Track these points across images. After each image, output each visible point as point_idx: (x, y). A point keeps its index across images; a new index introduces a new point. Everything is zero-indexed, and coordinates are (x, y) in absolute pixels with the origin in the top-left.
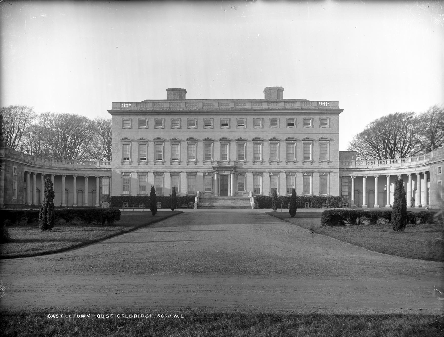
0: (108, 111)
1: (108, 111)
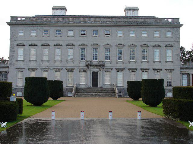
0: (183, 24)
1: (183, 24)
